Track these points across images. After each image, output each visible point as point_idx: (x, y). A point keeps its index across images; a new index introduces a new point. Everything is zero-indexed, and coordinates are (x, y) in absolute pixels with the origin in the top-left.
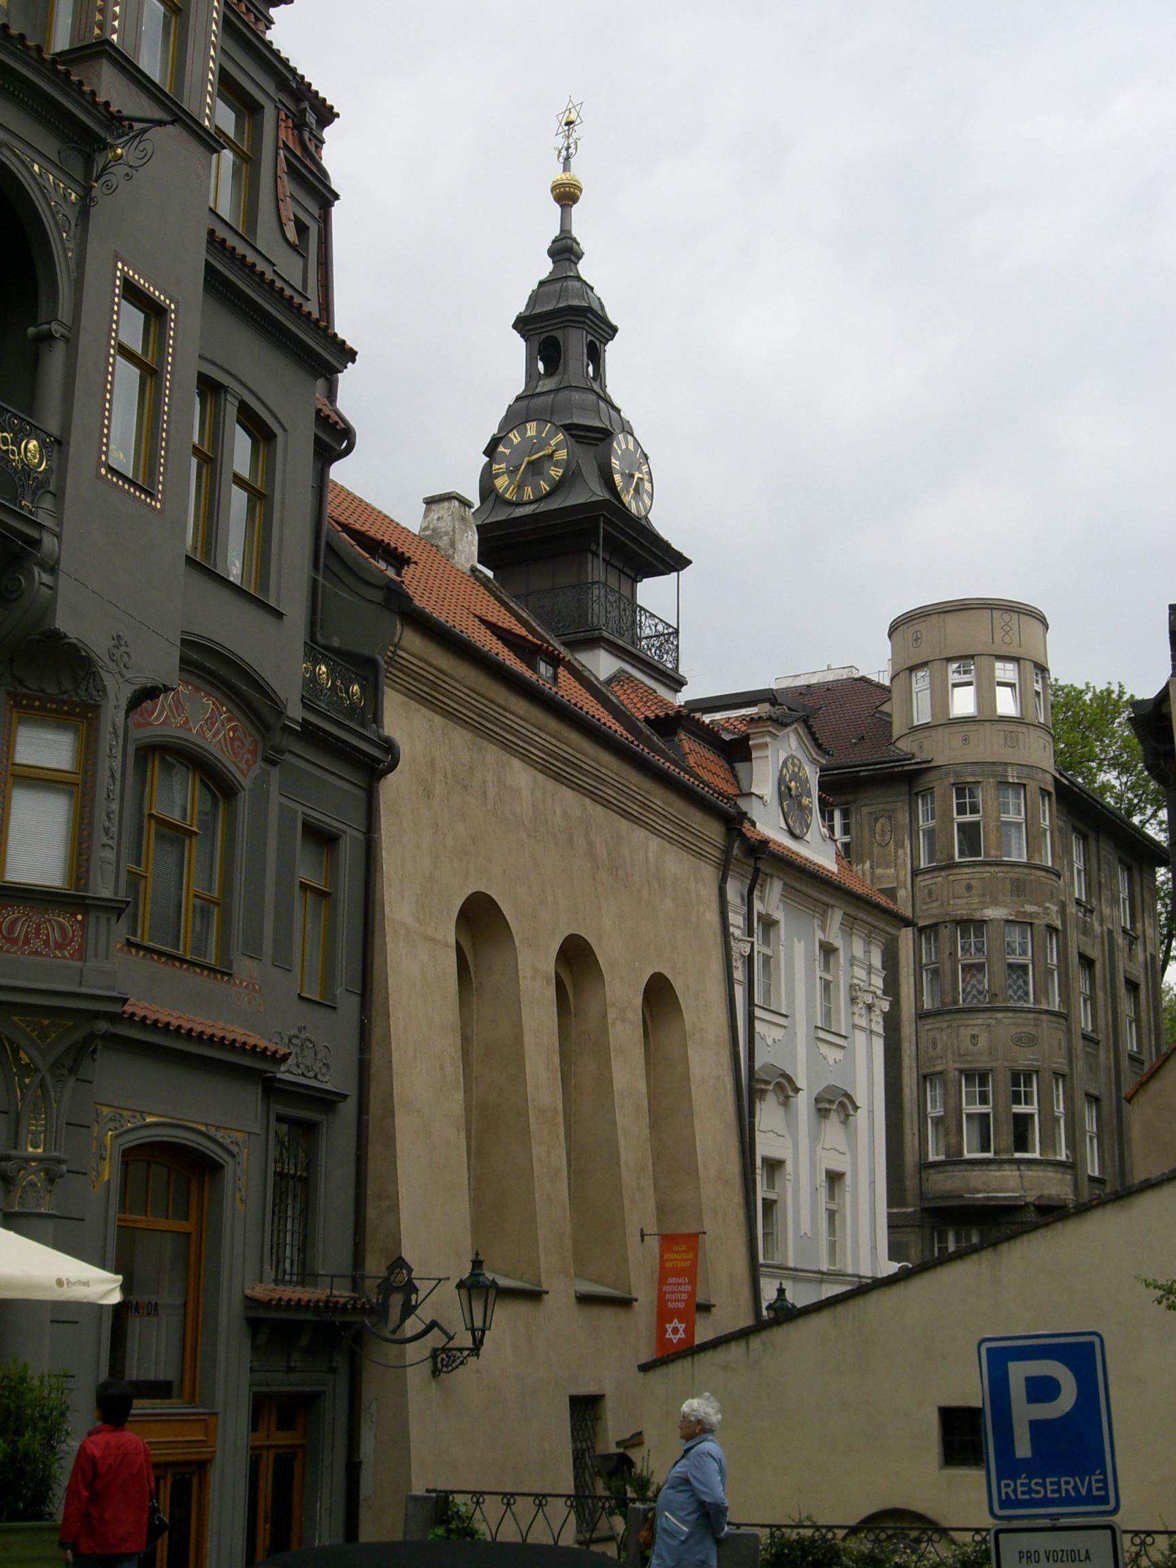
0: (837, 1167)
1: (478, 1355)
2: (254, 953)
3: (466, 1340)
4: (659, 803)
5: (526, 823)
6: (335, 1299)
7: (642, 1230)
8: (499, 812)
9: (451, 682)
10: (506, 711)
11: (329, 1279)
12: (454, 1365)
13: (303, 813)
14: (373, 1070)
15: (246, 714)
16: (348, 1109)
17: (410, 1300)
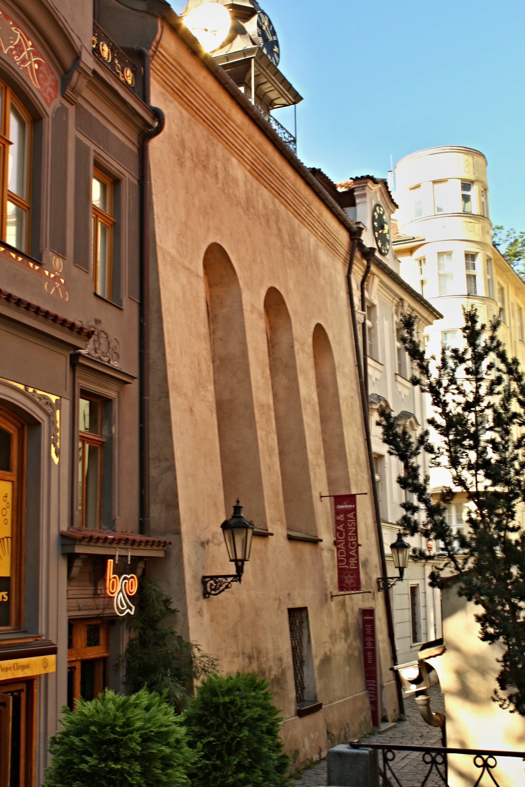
1: (240, 580)
2: (61, 253)
3: (232, 570)
5: (243, 203)
7: (320, 493)
8: (226, 191)
12: (221, 588)
13: (95, 151)
14: (151, 361)
15: (49, 56)
16: (134, 387)
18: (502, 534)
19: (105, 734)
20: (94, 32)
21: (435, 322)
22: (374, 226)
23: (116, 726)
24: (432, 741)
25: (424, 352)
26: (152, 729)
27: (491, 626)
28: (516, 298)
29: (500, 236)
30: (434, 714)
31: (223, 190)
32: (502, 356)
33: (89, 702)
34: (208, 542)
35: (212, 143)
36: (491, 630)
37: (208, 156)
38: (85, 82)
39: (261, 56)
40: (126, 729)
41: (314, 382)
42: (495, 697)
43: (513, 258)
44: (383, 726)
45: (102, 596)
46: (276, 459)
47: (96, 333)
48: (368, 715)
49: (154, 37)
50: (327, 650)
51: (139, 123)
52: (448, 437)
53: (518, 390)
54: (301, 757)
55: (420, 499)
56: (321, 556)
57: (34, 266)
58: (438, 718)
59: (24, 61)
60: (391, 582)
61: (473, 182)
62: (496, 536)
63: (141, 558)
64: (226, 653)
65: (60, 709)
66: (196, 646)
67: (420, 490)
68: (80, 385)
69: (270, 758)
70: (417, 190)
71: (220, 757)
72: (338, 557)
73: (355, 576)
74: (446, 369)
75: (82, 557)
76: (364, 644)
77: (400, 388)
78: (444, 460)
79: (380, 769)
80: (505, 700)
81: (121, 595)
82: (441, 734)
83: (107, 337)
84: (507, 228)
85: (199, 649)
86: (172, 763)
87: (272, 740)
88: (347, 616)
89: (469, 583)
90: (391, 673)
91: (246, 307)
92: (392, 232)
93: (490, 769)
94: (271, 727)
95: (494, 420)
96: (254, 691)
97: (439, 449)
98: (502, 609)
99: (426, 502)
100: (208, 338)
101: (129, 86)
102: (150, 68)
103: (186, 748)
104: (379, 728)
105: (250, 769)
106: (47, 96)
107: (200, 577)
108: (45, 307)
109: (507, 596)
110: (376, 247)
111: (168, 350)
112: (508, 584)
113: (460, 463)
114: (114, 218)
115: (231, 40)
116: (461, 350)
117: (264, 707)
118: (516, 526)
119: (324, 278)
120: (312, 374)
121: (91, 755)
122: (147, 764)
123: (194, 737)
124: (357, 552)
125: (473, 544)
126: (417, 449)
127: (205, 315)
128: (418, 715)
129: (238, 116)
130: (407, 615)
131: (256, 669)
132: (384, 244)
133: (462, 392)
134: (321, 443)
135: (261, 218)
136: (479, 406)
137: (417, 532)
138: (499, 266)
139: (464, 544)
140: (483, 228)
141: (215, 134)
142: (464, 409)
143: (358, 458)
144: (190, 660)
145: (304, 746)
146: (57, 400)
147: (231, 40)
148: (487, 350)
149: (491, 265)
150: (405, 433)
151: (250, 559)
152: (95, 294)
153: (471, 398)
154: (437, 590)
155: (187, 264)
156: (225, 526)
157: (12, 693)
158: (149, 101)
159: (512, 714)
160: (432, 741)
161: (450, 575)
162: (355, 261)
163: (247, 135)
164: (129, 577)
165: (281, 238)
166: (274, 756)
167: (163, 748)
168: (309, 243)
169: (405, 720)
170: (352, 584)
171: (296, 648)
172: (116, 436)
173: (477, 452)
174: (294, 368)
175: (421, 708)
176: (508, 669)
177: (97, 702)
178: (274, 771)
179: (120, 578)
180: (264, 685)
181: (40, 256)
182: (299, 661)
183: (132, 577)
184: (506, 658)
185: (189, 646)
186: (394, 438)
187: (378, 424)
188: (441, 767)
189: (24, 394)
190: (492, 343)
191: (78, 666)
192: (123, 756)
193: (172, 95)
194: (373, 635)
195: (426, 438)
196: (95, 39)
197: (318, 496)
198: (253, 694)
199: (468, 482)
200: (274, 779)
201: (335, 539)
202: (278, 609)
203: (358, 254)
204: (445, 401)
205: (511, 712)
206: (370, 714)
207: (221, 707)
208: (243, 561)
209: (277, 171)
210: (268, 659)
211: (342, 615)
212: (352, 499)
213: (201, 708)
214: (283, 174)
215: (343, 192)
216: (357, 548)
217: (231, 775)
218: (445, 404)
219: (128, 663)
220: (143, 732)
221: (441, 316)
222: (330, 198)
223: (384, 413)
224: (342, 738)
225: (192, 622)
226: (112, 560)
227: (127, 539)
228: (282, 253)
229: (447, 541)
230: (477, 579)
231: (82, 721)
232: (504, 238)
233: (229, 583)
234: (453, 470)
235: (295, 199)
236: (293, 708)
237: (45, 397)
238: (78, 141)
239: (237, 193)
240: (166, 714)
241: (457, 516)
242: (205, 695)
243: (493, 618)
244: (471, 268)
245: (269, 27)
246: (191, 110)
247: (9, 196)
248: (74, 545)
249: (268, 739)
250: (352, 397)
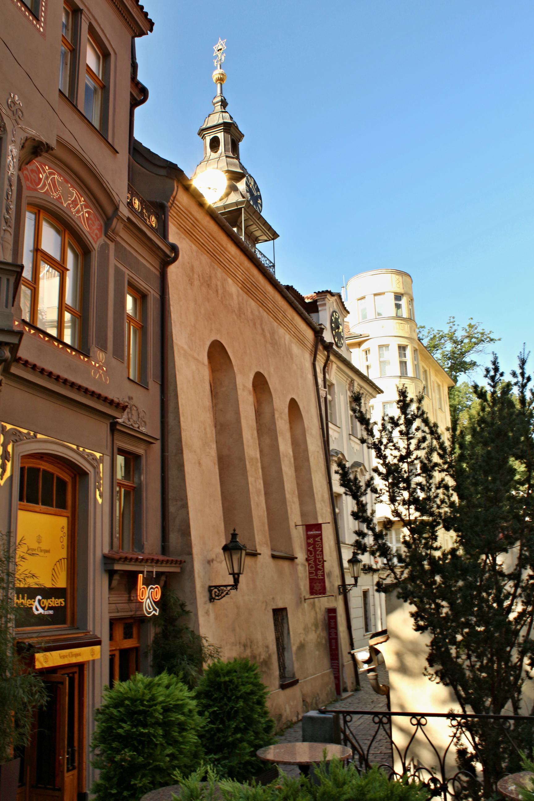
1: (236, 589)
2: (104, 348)
3: (230, 580)
5: (236, 311)
9: (201, 227)
13: (128, 275)
14: (170, 427)
15: (96, 207)
16: (157, 446)
18: (429, 552)
19: (136, 706)
20: (129, 191)
21: (378, 396)
22: (332, 327)
23: (144, 700)
24: (381, 705)
25: (369, 419)
26: (171, 702)
27: (422, 620)
28: (435, 378)
29: (423, 333)
30: (381, 685)
31: (222, 302)
32: (426, 421)
33: (124, 683)
34: (212, 560)
35: (214, 268)
36: (421, 623)
37: (210, 277)
38: (122, 226)
39: (249, 205)
40: (152, 703)
41: (289, 441)
42: (425, 672)
43: (433, 349)
44: (345, 695)
45: (135, 601)
46: (263, 498)
47: (129, 407)
48: (332, 686)
49: (172, 194)
50: (302, 639)
51: (160, 254)
52: (388, 481)
53: (438, 447)
54: (284, 719)
55: (368, 528)
56: (296, 569)
57: (84, 358)
58: (384, 688)
59: (78, 212)
60: (349, 588)
61: (402, 295)
62: (424, 554)
63: (163, 573)
64: (227, 643)
65: (103, 688)
66: (205, 638)
67: (368, 521)
69: (259, 722)
70: (363, 300)
71: (222, 722)
72: (309, 570)
73: (322, 584)
74: (385, 431)
75: (119, 572)
76: (330, 634)
77: (353, 444)
78: (386, 497)
79: (341, 728)
80: (433, 675)
81: (148, 600)
82: (386, 700)
84: (427, 327)
85: (207, 640)
86: (186, 727)
87: (260, 708)
88: (316, 613)
89: (405, 589)
90: (349, 656)
92: (345, 330)
93: (422, 726)
94: (260, 699)
95: (421, 469)
96: (247, 672)
97: (381, 490)
98: (430, 608)
99: (373, 529)
100: (211, 410)
101: (154, 228)
102: (168, 215)
103: (197, 717)
104: (341, 696)
105: (244, 731)
106: (95, 236)
107: (207, 587)
108: (92, 388)
109: (433, 598)
110: (333, 342)
111: (182, 419)
112: (433, 589)
113: (396, 501)
114: (142, 323)
115: (227, 195)
116: (396, 418)
117: (255, 685)
118: (438, 546)
119: (296, 365)
120: (288, 435)
121: (126, 723)
122: (168, 729)
123: (203, 708)
124: (323, 566)
125: (408, 560)
126: (365, 490)
127: (210, 393)
128: (370, 686)
129: (232, 249)
130: (361, 612)
131: (249, 654)
132: (339, 340)
133: (397, 448)
134: (296, 486)
135: (250, 321)
136: (410, 458)
137: (366, 551)
138: (423, 355)
139: (400, 560)
140: (411, 328)
142: (399, 461)
143: (323, 496)
144: (200, 649)
145: (286, 711)
146: (100, 456)
147: (227, 195)
148: (415, 417)
149: (417, 354)
150: (356, 478)
151: (244, 573)
152: (129, 378)
153: (404, 452)
154: (383, 595)
155: (196, 355)
156: (225, 549)
157: (68, 674)
158: (168, 239)
159: (438, 685)
160: (381, 705)
161: (390, 582)
162: (318, 352)
163: (239, 262)
164: (154, 587)
165: (265, 337)
166: (263, 720)
167: (179, 716)
168: (285, 340)
169: (360, 690)
170: (320, 590)
171: (279, 638)
172: (144, 482)
173: (409, 492)
174: (275, 430)
175: (371, 681)
176: (434, 652)
177: (130, 683)
178: (263, 732)
179: (147, 588)
180: (255, 667)
181: (89, 351)
182: (281, 648)
183: (157, 587)
184: (433, 643)
185: (197, 638)
186: (349, 483)
187: (336, 472)
188: (387, 727)
189: (76, 452)
190: (418, 412)
191: (117, 654)
192: (149, 723)
193: (185, 235)
194: (336, 627)
195: (372, 482)
196: (129, 196)
197: (294, 525)
198: (247, 674)
199: (403, 515)
200: (263, 738)
201: (306, 556)
202: (265, 610)
203: (320, 347)
204: (385, 455)
205: (438, 683)
206: (334, 686)
207: (223, 685)
208: (239, 574)
209: (261, 287)
210: (258, 647)
211: (313, 613)
212: (319, 527)
213: (208, 686)
214: (265, 290)
215: (309, 303)
216: (323, 563)
217: (230, 736)
218: (385, 457)
219: (155, 651)
220: (164, 704)
221: (382, 392)
222: (300, 306)
223: (341, 465)
224: (314, 705)
225: (202, 620)
226: (141, 575)
227: (153, 559)
228: (265, 347)
229: (388, 558)
230: (411, 585)
231: (119, 697)
232: (427, 335)
233: (229, 591)
234: (392, 506)
236: (277, 683)
237: (91, 454)
238: (116, 268)
239: (232, 304)
240: (181, 691)
241: (396, 538)
242: (211, 676)
243: (423, 614)
244: (403, 356)
245: (254, 186)
246: (198, 245)
247: (66, 307)
248: (113, 564)
249: (258, 708)
250: (318, 452)
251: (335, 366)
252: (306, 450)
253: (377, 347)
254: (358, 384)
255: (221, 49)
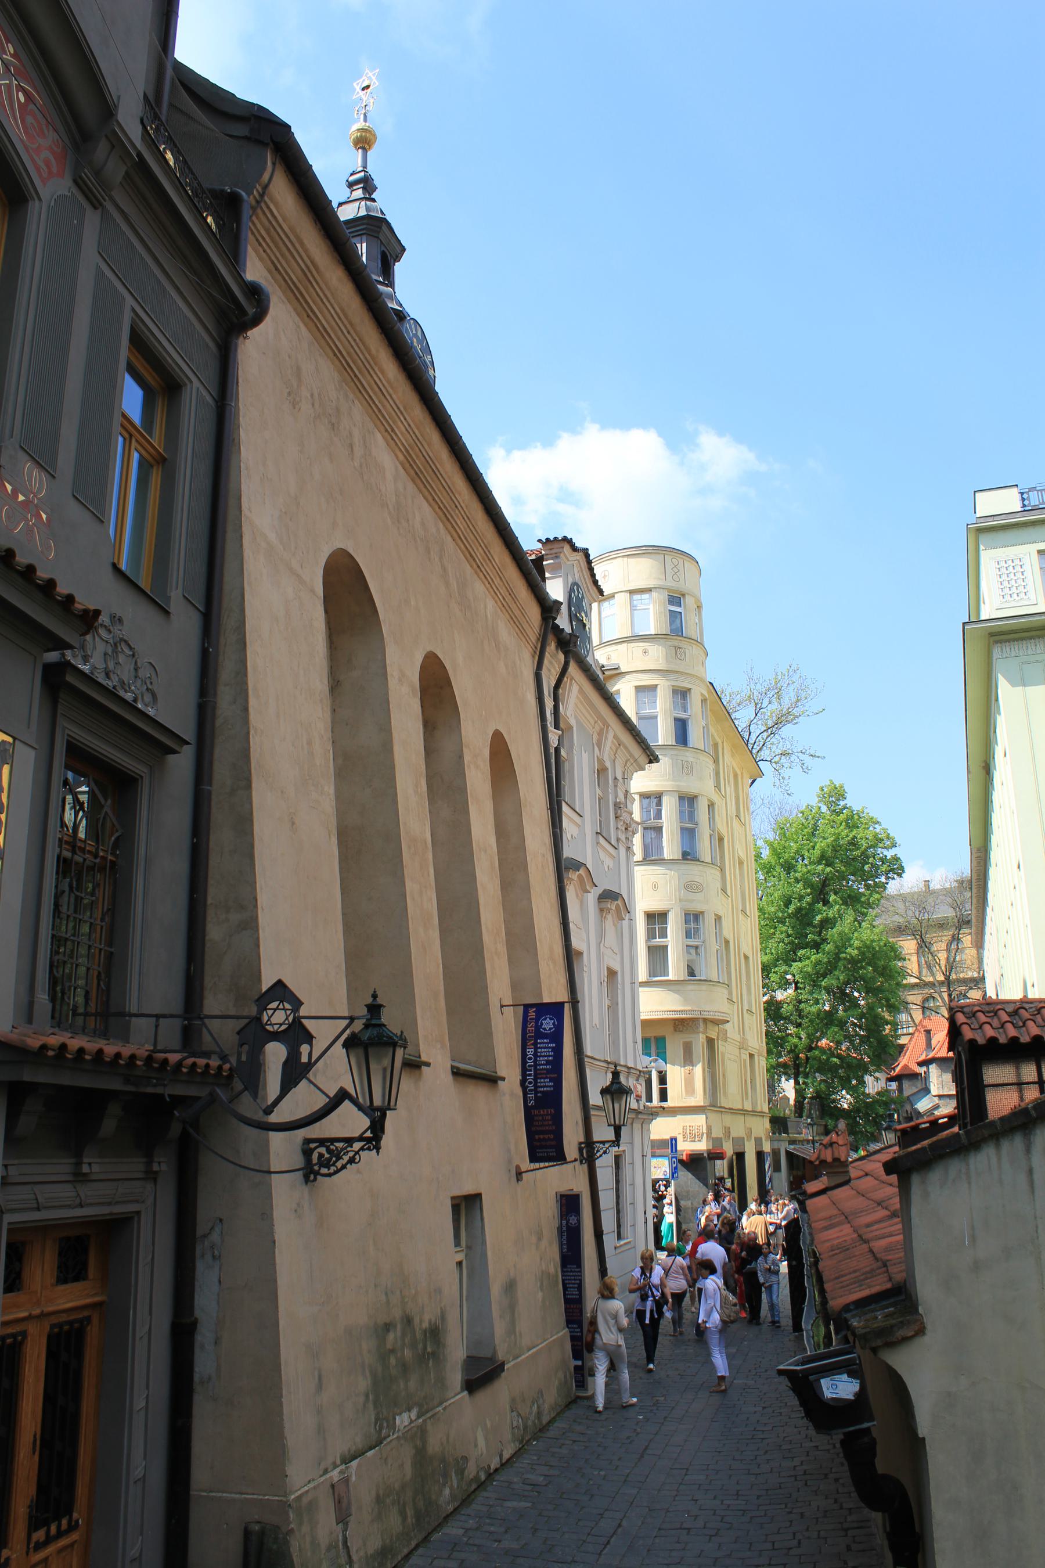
0: (616, 967)
1: (378, 1148)
4: (497, 561)
5: (391, 507)
6: (162, 1055)
10: (376, 364)
11: (154, 1019)
12: (339, 1164)
13: (133, 310)
14: (219, 722)
17: (299, 1054)
49: (261, 175)
68: (67, 731)
83: (133, 655)
91: (392, 671)
111: (252, 702)
120: (489, 806)
141: (352, 384)
152: (115, 567)
165: (447, 584)
174: (463, 790)
203: (552, 647)
208: (383, 1112)
233: (357, 1153)
235: (468, 530)
251: (576, 686)
252: (522, 847)
253: (633, 690)
254: (615, 737)
255: (368, 87)
